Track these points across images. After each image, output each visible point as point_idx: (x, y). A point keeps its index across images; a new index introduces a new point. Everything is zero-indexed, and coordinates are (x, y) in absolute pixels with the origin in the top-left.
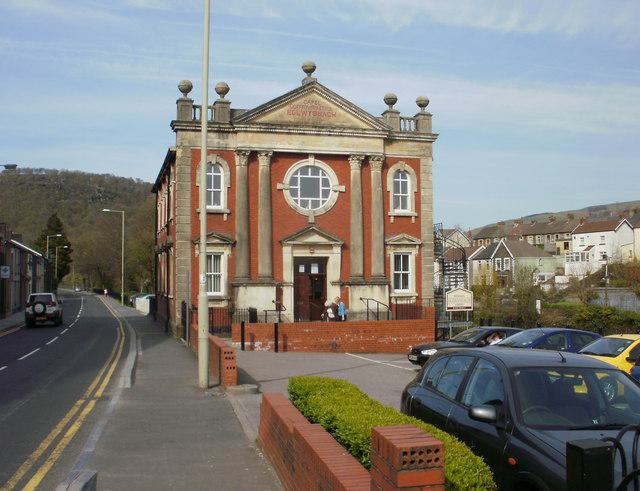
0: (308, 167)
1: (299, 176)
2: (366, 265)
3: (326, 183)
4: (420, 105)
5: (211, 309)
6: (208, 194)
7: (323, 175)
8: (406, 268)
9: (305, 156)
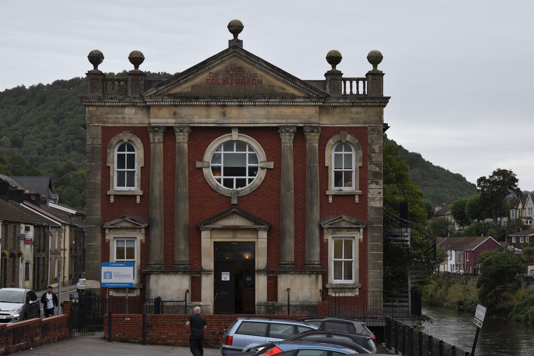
0: (233, 141)
1: (222, 152)
3: (254, 158)
6: (121, 175)
8: (349, 255)
9: (228, 130)
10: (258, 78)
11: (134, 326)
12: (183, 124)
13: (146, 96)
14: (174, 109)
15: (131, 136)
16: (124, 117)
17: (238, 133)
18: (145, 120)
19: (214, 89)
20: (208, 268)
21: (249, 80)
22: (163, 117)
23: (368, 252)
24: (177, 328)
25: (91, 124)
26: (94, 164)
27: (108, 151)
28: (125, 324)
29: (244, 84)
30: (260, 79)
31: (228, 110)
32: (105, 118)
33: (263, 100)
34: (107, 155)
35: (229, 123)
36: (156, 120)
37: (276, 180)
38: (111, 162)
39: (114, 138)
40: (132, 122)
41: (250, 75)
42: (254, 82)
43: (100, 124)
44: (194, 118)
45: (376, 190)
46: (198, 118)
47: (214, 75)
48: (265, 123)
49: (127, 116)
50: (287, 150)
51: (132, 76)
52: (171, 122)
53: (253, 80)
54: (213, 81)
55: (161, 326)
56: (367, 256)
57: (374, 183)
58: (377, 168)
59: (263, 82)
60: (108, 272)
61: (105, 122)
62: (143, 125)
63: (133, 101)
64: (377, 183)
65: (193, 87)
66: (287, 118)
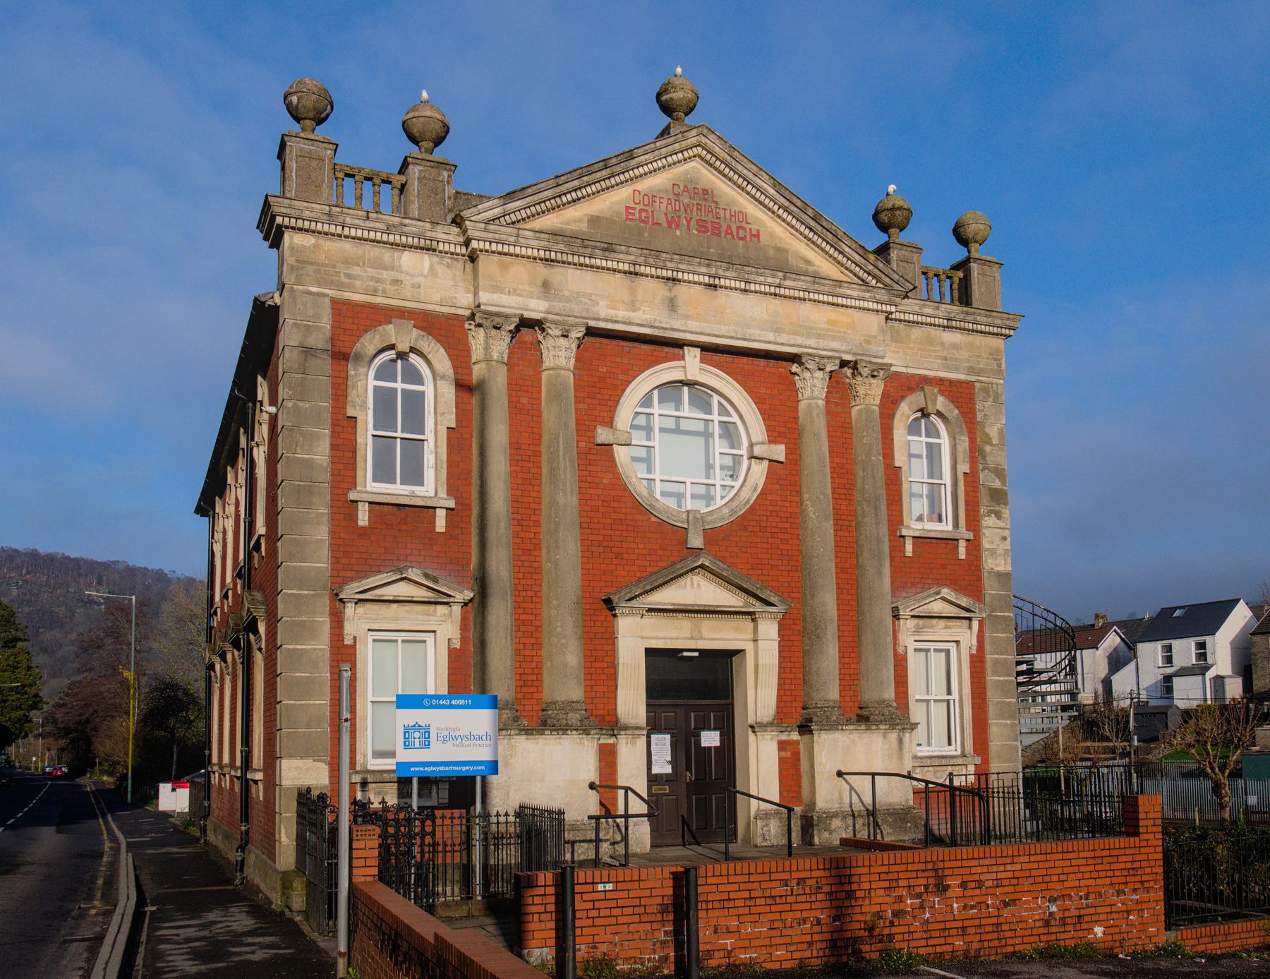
2: (850, 677)
4: (884, 227)
5: (474, 778)
6: (384, 445)
7: (723, 411)
9: (672, 346)
10: (750, 226)
11: (626, 911)
12: (566, 318)
13: (473, 218)
14: (543, 271)
15: (420, 335)
16: (398, 281)
17: (701, 362)
18: (457, 295)
19: (646, 235)
20: (633, 722)
21: (729, 227)
22: (515, 290)
23: (988, 678)
24: (767, 909)
25: (301, 288)
26: (307, 405)
27: (352, 373)
28: (597, 905)
29: (719, 235)
30: (754, 227)
31: (682, 291)
32: (342, 275)
33: (770, 280)
34: (350, 383)
35: (684, 331)
36: (496, 297)
37: (788, 493)
38: (361, 406)
39: (368, 336)
40: (422, 299)
41: (731, 215)
42: (741, 234)
43: (327, 291)
44: (598, 304)
45: (997, 530)
46: (608, 307)
47: (646, 198)
48: (770, 342)
49: (408, 277)
50: (818, 415)
51: (421, 168)
52: (536, 308)
53: (739, 228)
54: (644, 214)
55: (716, 905)
56: (985, 688)
57: (993, 515)
58: (997, 480)
59: (762, 237)
60: (417, 727)
61: (341, 286)
62: (453, 311)
63: (429, 234)
64: (998, 515)
65: (594, 221)
66: (819, 336)
